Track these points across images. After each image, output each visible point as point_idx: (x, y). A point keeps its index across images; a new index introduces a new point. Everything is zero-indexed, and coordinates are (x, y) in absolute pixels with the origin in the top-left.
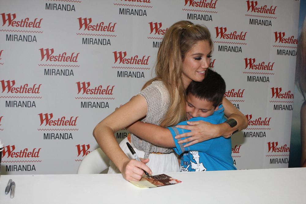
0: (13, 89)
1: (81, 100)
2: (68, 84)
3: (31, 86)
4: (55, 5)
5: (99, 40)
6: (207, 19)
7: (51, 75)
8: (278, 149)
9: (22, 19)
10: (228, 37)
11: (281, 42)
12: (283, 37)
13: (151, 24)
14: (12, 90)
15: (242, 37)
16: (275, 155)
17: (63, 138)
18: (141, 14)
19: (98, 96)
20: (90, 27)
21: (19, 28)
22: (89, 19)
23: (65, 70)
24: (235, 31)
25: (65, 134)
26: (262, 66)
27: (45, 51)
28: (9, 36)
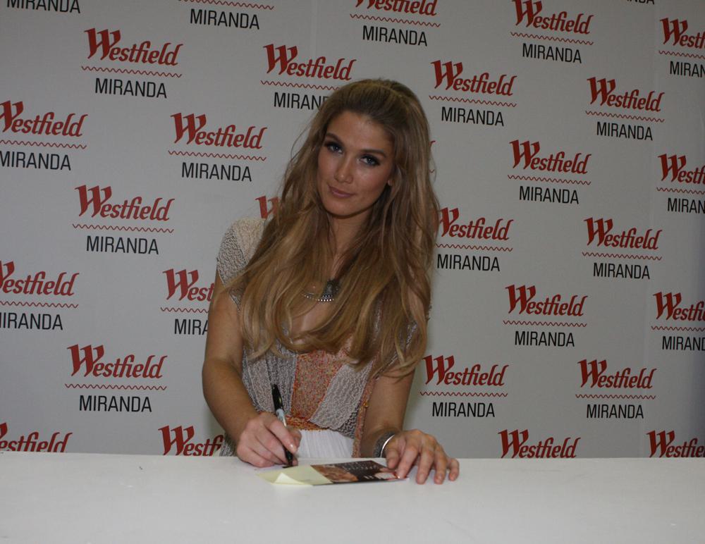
0: (202, 135)
3: (241, 130)
7: (102, 250)
9: (134, 43)
12: (608, 231)
13: (437, 64)
18: (413, 41)
22: (8, 265)
24: (482, 217)
26: (629, 239)
28: (102, 82)
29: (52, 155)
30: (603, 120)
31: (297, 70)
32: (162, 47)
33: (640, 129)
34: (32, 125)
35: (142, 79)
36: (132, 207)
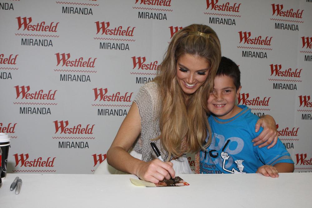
1: (209, 16)
2: (124, 59)
3: (125, 28)
4: (31, 41)
5: (117, 44)
6: (230, 23)
7: (67, 80)
8: (307, 162)
10: (253, 42)
11: (309, 47)
14: (27, 96)
15: (267, 42)
16: (304, 168)
17: (118, 115)
19: (116, 103)
20: (108, 31)
21: (35, 32)
23: (42, 109)
25: (81, 142)
26: (288, 73)
27: (101, 24)
28: (65, 8)
29: (45, 40)
30: (245, 50)
31: (110, 32)
32: (9, 56)
33: (293, 26)
34: (36, 27)
35: (42, 39)
36: (79, 62)
